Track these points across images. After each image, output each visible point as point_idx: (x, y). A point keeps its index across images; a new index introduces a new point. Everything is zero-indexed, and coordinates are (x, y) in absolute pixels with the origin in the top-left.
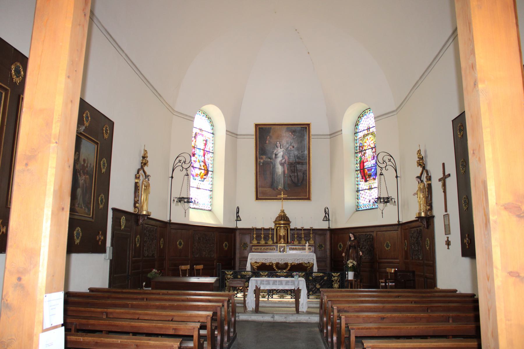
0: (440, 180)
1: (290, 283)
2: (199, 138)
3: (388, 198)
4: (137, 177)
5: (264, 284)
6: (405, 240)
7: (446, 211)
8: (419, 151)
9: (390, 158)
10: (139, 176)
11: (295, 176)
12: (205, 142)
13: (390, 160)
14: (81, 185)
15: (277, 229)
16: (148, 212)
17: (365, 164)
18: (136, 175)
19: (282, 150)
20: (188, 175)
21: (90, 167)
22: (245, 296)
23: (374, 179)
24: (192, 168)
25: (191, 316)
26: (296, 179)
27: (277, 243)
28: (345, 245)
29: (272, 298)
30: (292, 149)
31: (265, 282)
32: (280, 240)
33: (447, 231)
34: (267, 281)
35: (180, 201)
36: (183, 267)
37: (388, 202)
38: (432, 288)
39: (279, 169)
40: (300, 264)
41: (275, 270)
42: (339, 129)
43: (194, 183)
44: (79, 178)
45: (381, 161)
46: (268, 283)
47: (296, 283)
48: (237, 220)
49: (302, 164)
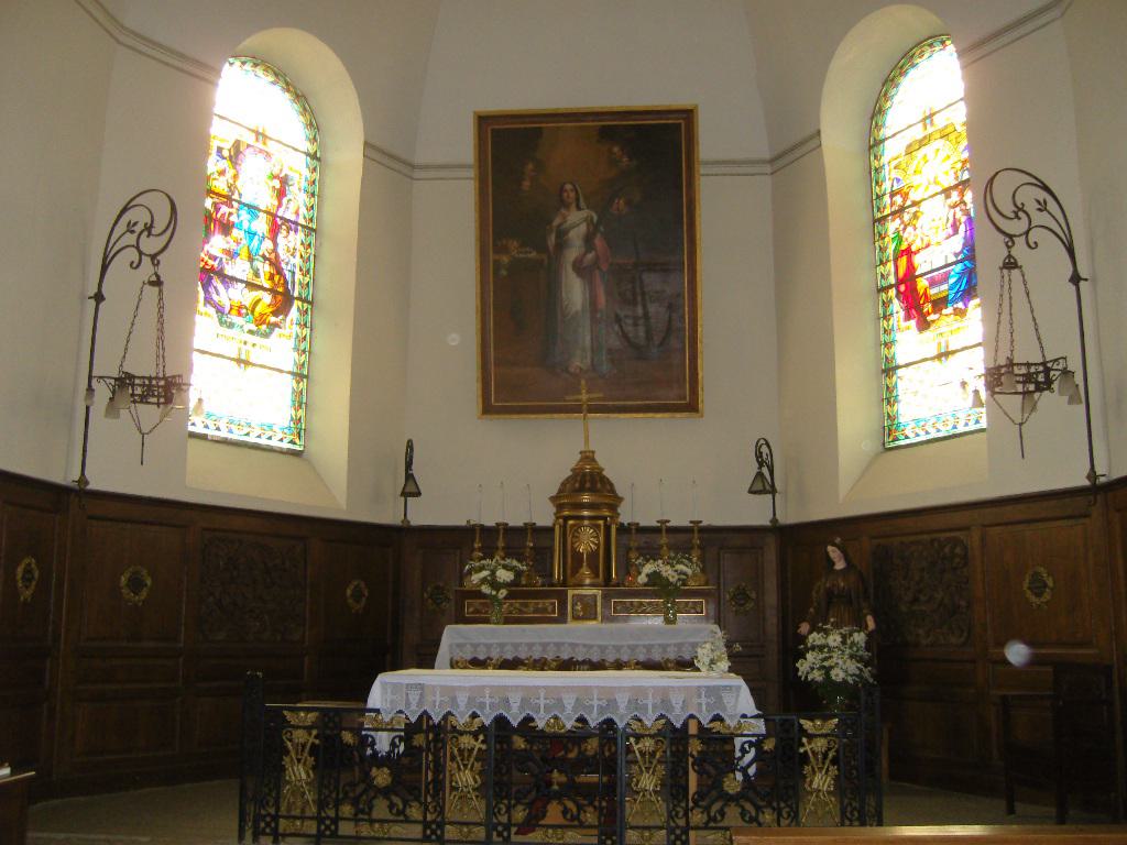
2: (252, 165)
9: (1043, 195)
11: (636, 319)
12: (277, 184)
13: (1043, 207)
15: (564, 527)
17: (917, 260)
23: (960, 313)
26: (641, 332)
27: (564, 584)
32: (576, 570)
45: (1008, 209)
49: (664, 269)
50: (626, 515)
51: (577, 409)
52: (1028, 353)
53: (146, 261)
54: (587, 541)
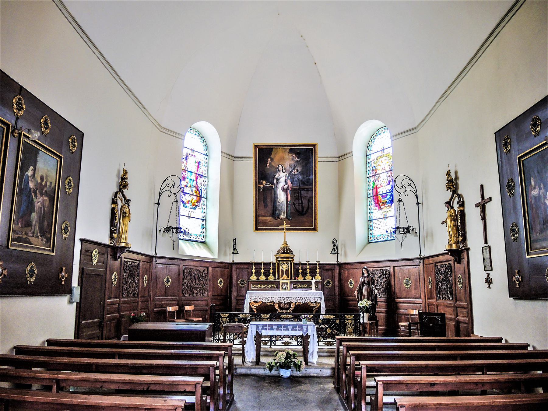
0: (477, 206)
1: (297, 329)
2: (191, 160)
3: (408, 228)
4: (114, 202)
5: (266, 329)
6: (428, 277)
7: (486, 242)
8: (448, 173)
10: (117, 200)
11: (299, 204)
12: (197, 164)
13: (409, 185)
14: (36, 209)
15: (278, 264)
16: (127, 243)
17: (379, 190)
18: (113, 199)
19: (285, 173)
20: (177, 201)
21: (50, 186)
22: (243, 343)
23: (390, 207)
24: (182, 194)
25: (174, 384)
26: (300, 207)
28: (356, 282)
29: (275, 345)
30: (296, 173)
31: (268, 328)
33: (488, 265)
34: (269, 325)
35: (167, 231)
36: (170, 309)
37: (408, 232)
38: (469, 336)
39: (281, 196)
40: (306, 304)
41: (277, 310)
42: (350, 151)
43: (184, 211)
44: (35, 200)
45: (400, 186)
46: (271, 327)
47: (305, 328)
48: (233, 254)
49: (308, 190)
50: (296, 260)
51: (283, 229)
52: (403, 224)
53: (173, 195)
54: (285, 267)
